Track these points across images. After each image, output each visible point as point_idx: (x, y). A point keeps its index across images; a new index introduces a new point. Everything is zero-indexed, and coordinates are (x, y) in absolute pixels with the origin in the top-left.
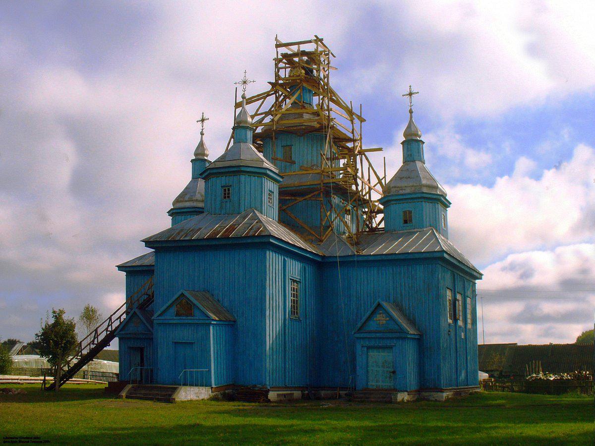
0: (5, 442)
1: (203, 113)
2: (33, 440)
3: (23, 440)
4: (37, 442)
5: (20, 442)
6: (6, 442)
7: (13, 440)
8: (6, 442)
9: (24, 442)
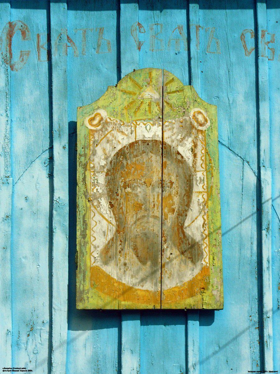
0: (3, 371)
1: (31, 371)
2: (21, 370)
3: (15, 370)
4: (24, 371)
5: (13, 371)
6: (5, 371)
7: (9, 370)
8: (5, 371)
9: (16, 371)
